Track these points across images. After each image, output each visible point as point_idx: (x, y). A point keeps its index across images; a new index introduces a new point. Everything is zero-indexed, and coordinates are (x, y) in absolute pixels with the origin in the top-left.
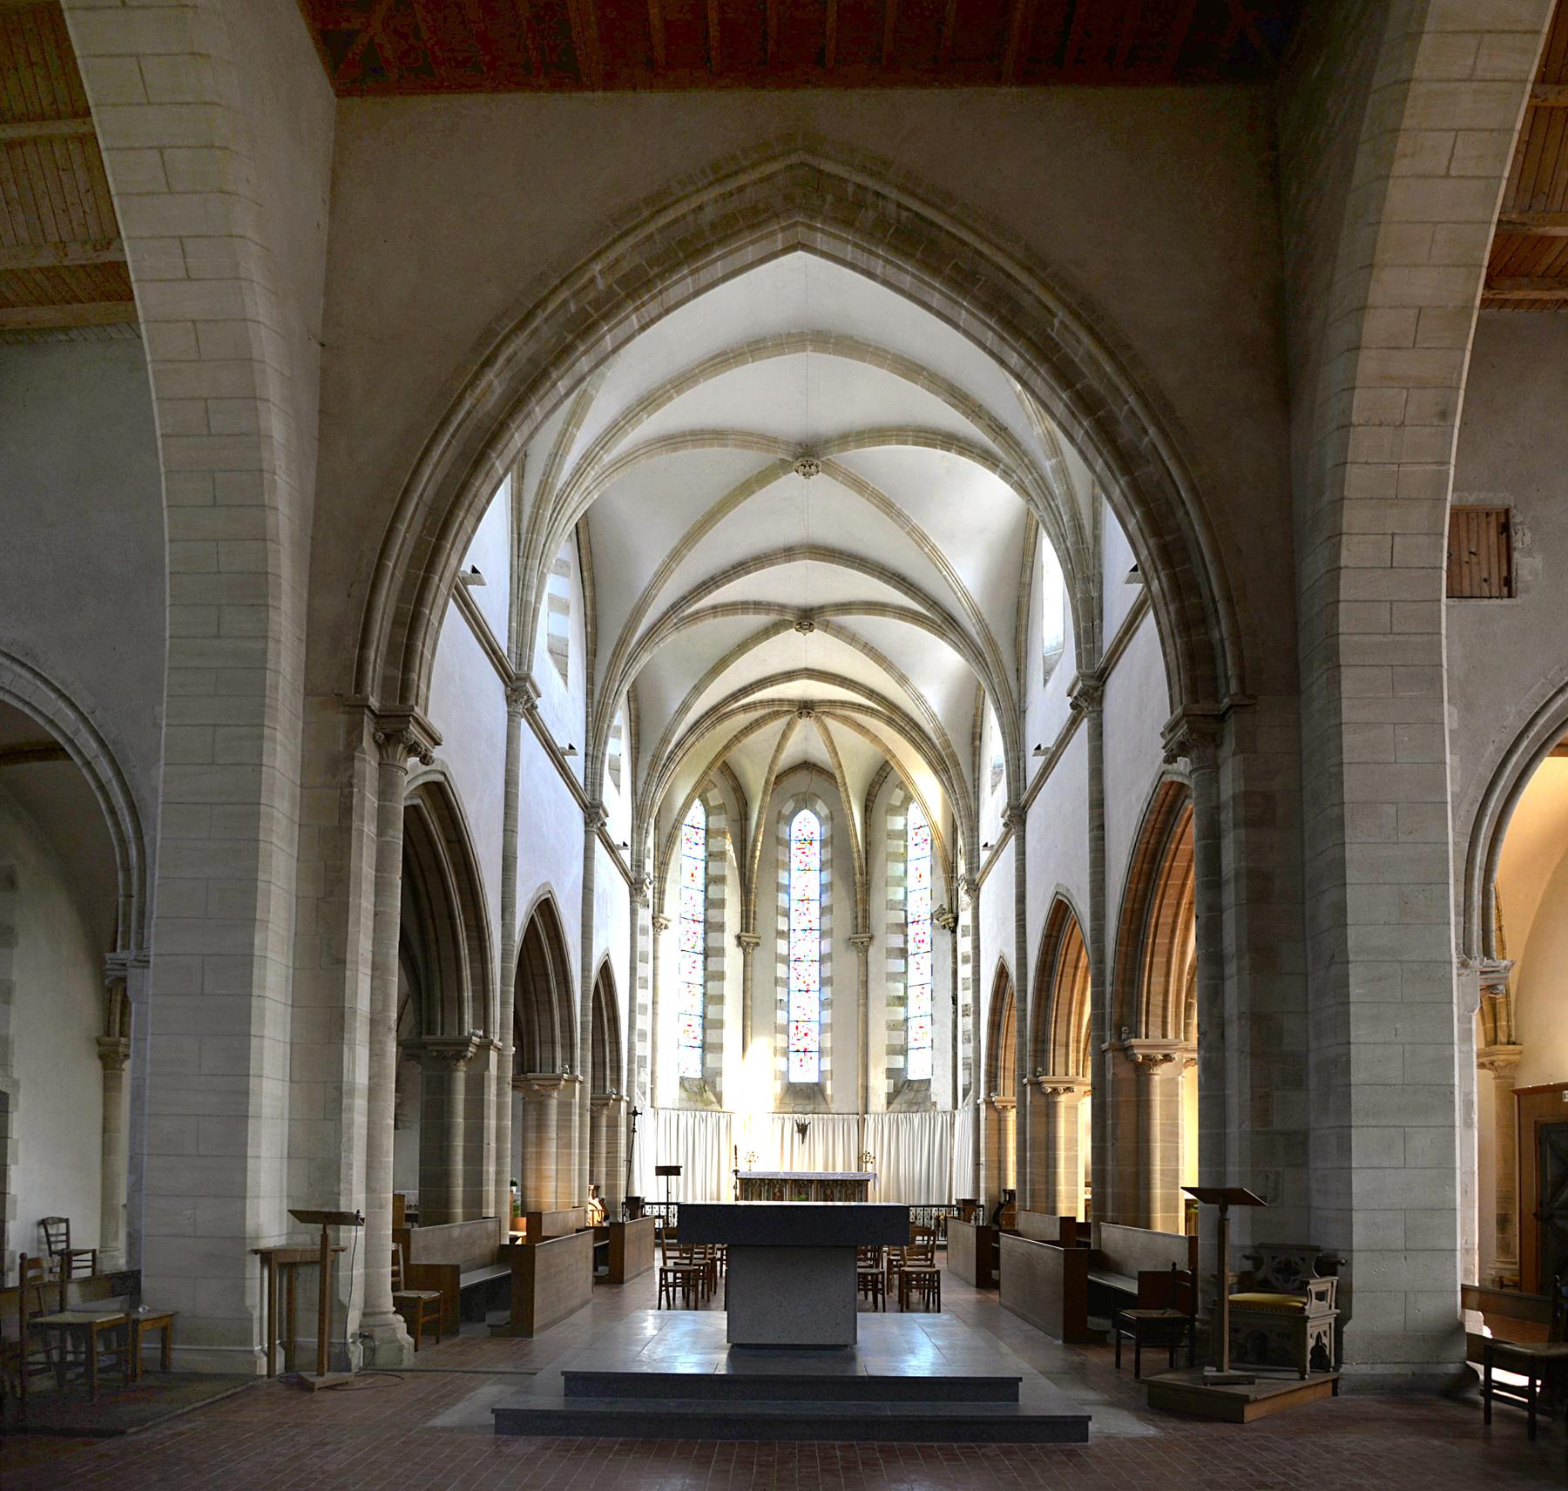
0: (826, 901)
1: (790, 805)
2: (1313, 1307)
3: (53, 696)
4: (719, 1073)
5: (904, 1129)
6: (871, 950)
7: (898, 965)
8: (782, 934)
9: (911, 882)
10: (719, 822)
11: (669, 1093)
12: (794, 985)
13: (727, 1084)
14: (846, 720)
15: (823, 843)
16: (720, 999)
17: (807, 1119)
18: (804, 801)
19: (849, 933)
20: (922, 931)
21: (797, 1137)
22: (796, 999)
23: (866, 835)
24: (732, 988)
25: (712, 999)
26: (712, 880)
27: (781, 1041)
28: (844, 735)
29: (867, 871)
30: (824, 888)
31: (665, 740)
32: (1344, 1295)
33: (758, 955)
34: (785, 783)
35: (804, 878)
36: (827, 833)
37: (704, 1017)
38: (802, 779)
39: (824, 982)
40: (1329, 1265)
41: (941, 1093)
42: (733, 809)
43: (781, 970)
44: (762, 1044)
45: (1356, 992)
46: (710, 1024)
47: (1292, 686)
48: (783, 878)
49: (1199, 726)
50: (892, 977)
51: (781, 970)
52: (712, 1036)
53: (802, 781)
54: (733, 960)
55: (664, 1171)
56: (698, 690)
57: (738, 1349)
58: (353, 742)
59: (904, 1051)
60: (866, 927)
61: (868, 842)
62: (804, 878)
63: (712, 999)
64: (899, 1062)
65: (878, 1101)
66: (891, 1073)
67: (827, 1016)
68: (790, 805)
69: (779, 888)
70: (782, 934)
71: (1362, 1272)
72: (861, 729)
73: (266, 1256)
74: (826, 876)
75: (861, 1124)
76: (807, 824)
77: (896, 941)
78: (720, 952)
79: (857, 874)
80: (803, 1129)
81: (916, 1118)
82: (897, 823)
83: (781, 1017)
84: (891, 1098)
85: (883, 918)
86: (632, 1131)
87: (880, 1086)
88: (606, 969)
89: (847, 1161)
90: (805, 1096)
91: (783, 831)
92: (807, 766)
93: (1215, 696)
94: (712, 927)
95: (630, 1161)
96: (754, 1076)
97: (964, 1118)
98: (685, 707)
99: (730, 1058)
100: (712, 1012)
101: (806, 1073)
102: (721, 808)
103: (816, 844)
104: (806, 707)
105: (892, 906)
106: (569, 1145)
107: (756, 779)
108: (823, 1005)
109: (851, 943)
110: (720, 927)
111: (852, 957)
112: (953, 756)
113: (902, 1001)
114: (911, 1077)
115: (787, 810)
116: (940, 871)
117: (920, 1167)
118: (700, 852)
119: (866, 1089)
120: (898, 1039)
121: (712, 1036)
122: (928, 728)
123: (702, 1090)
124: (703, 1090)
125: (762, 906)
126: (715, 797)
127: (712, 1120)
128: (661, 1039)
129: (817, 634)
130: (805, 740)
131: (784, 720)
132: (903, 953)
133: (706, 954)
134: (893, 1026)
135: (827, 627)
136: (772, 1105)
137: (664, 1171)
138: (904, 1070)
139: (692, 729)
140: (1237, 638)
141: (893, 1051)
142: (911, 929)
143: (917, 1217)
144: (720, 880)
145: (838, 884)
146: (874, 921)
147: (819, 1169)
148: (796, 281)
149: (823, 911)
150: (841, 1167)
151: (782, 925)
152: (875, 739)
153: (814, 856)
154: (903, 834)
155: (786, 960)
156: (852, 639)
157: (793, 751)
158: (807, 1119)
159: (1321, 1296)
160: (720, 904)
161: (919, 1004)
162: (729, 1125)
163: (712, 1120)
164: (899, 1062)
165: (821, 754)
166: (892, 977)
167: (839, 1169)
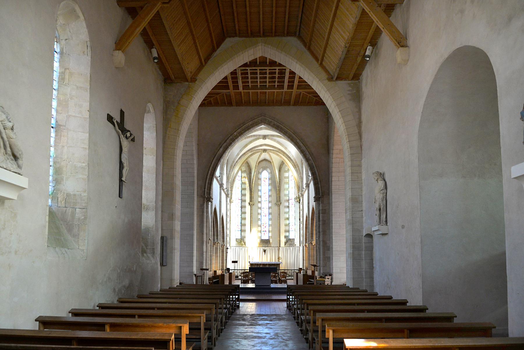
0: (270, 193)
1: (261, 169)
2: (326, 280)
3: (124, 171)
4: (245, 237)
5: (289, 251)
6: (281, 206)
7: (287, 210)
8: (259, 202)
9: (290, 189)
10: (244, 175)
11: (233, 243)
12: (262, 214)
13: (246, 240)
14: (274, 153)
15: (269, 179)
16: (245, 219)
17: (266, 248)
18: (265, 168)
19: (275, 202)
20: (292, 202)
21: (263, 253)
22: (263, 218)
23: (279, 178)
24: (248, 216)
25: (243, 219)
26: (243, 189)
27: (259, 228)
28: (274, 156)
29: (280, 187)
30: (270, 190)
31: (233, 162)
32: (332, 279)
33: (254, 207)
34: (260, 164)
35: (265, 187)
36: (270, 177)
37: (241, 223)
38: (264, 162)
39: (270, 214)
40: (331, 275)
41: (297, 242)
42: (248, 171)
43: (259, 211)
44: (255, 229)
45: (333, 238)
46: (243, 225)
47: (329, 195)
48: (260, 188)
49: (317, 199)
50: (286, 213)
51: (259, 211)
52: (243, 228)
53: (264, 164)
54: (248, 208)
55: (233, 262)
56: (241, 151)
57: (256, 286)
58: (204, 203)
59: (288, 231)
60: (280, 200)
61: (280, 179)
62: (265, 187)
63: (243, 219)
64: (287, 234)
65: (282, 244)
66: (286, 237)
67: (270, 223)
68: (261, 169)
69: (259, 190)
70: (259, 202)
71: (334, 276)
72: (278, 155)
73: (195, 275)
74: (270, 188)
75: (279, 250)
76: (265, 175)
77: (287, 204)
78: (245, 207)
79: (277, 187)
80: (265, 251)
81: (291, 248)
82: (286, 175)
83: (259, 223)
84: (285, 243)
85: (283, 198)
86: (227, 253)
87: (283, 240)
88: (215, 209)
89: (275, 260)
90: (265, 243)
91: (260, 176)
92: (265, 160)
93: (319, 195)
94: (243, 201)
95: (226, 260)
96: (253, 239)
97: (301, 248)
98: (238, 154)
99: (247, 234)
100: (243, 222)
101: (265, 237)
102: (245, 171)
103: (268, 179)
104: (265, 151)
105: (285, 195)
106: (217, 257)
107: (253, 165)
108: (270, 219)
109: (276, 204)
110: (245, 201)
111: (276, 208)
112: (297, 165)
113: (288, 219)
114: (290, 238)
115: (260, 171)
116: (296, 188)
117: (292, 261)
118: (240, 182)
119: (280, 241)
120: (287, 228)
121: (243, 228)
122: (292, 158)
123: (241, 241)
124: (241, 241)
125: (255, 195)
126: (243, 169)
127: (243, 249)
128: (233, 232)
129: (267, 140)
130: (264, 156)
131: (260, 153)
132: (288, 207)
133: (242, 208)
134: (286, 225)
135: (269, 139)
136: (258, 245)
137: (233, 262)
138: (289, 236)
139: (239, 158)
140: (321, 187)
141: (287, 231)
142: (290, 201)
143: (289, 273)
144: (245, 189)
145: (273, 190)
146: (281, 199)
147: (269, 261)
148: (263, 130)
149: (269, 196)
150: (274, 261)
151: (260, 200)
152: (281, 157)
153: (267, 182)
154: (288, 177)
155: (260, 208)
156: (275, 140)
157: (262, 157)
158: (266, 248)
159: (328, 279)
160: (245, 195)
161: (292, 221)
162: (247, 250)
163: (243, 249)
164: (287, 234)
165: (268, 158)
166: (286, 213)
167: (274, 261)
